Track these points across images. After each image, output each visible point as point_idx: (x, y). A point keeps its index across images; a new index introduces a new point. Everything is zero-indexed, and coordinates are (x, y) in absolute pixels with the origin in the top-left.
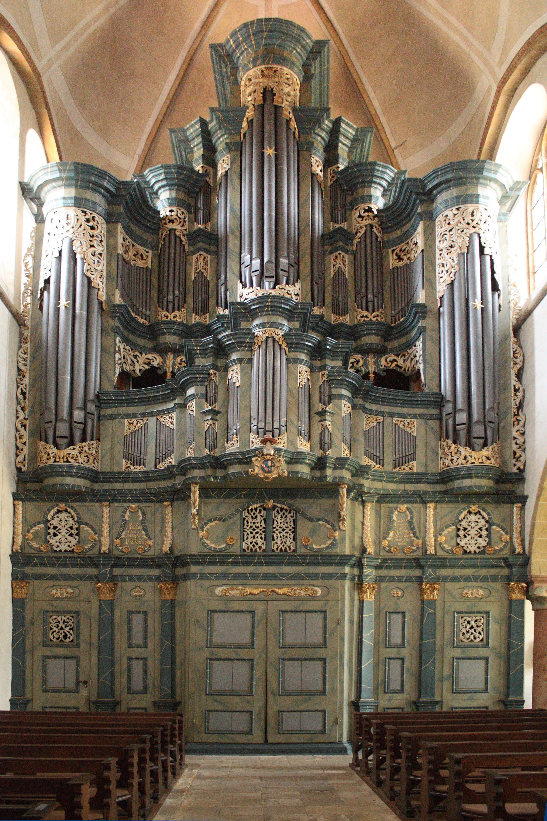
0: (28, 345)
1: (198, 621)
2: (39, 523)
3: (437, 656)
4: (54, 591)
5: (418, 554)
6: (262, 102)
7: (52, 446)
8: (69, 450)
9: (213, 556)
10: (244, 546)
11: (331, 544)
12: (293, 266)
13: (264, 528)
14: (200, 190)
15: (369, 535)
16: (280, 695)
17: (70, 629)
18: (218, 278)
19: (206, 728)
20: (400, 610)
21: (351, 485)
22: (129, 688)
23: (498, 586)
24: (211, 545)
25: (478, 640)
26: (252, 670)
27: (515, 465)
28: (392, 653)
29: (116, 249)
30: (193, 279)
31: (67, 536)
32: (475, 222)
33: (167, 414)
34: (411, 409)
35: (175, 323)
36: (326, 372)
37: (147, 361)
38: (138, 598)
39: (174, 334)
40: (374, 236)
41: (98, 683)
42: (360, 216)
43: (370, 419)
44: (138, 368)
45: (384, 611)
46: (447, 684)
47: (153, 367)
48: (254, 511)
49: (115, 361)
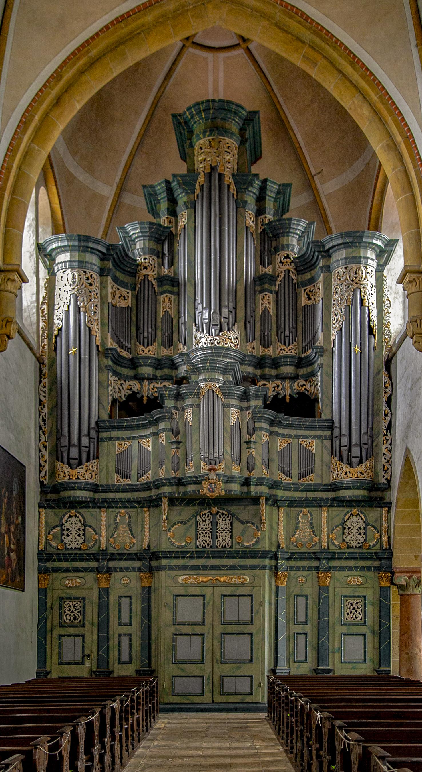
0: (46, 380)
1: (167, 604)
2: (57, 526)
3: (330, 632)
4: (67, 582)
5: (316, 549)
6: (210, 171)
7: (67, 466)
8: (78, 470)
9: (177, 552)
10: (198, 544)
11: (256, 541)
12: (231, 312)
13: (211, 529)
14: (166, 239)
15: (282, 533)
16: (222, 663)
17: (78, 612)
18: (179, 317)
19: (173, 690)
20: (304, 594)
21: (268, 496)
22: (119, 659)
23: (371, 574)
24: (176, 543)
25: (358, 619)
26: (203, 643)
27: (384, 476)
28: (298, 629)
29: (107, 300)
30: (161, 316)
31: (76, 536)
32: (358, 279)
33: (146, 439)
34: (312, 432)
35: (149, 358)
36: (250, 411)
37: (129, 388)
38: (126, 585)
39: (149, 366)
40: (290, 279)
41: (98, 655)
42: (281, 262)
43: (283, 441)
44: (123, 393)
45: (293, 594)
46: (337, 655)
47: (134, 392)
48: (204, 516)
49: (108, 393)
